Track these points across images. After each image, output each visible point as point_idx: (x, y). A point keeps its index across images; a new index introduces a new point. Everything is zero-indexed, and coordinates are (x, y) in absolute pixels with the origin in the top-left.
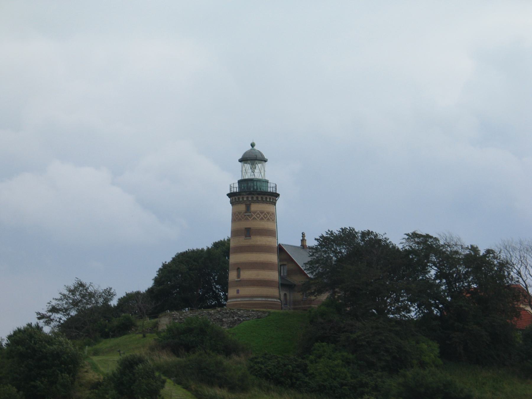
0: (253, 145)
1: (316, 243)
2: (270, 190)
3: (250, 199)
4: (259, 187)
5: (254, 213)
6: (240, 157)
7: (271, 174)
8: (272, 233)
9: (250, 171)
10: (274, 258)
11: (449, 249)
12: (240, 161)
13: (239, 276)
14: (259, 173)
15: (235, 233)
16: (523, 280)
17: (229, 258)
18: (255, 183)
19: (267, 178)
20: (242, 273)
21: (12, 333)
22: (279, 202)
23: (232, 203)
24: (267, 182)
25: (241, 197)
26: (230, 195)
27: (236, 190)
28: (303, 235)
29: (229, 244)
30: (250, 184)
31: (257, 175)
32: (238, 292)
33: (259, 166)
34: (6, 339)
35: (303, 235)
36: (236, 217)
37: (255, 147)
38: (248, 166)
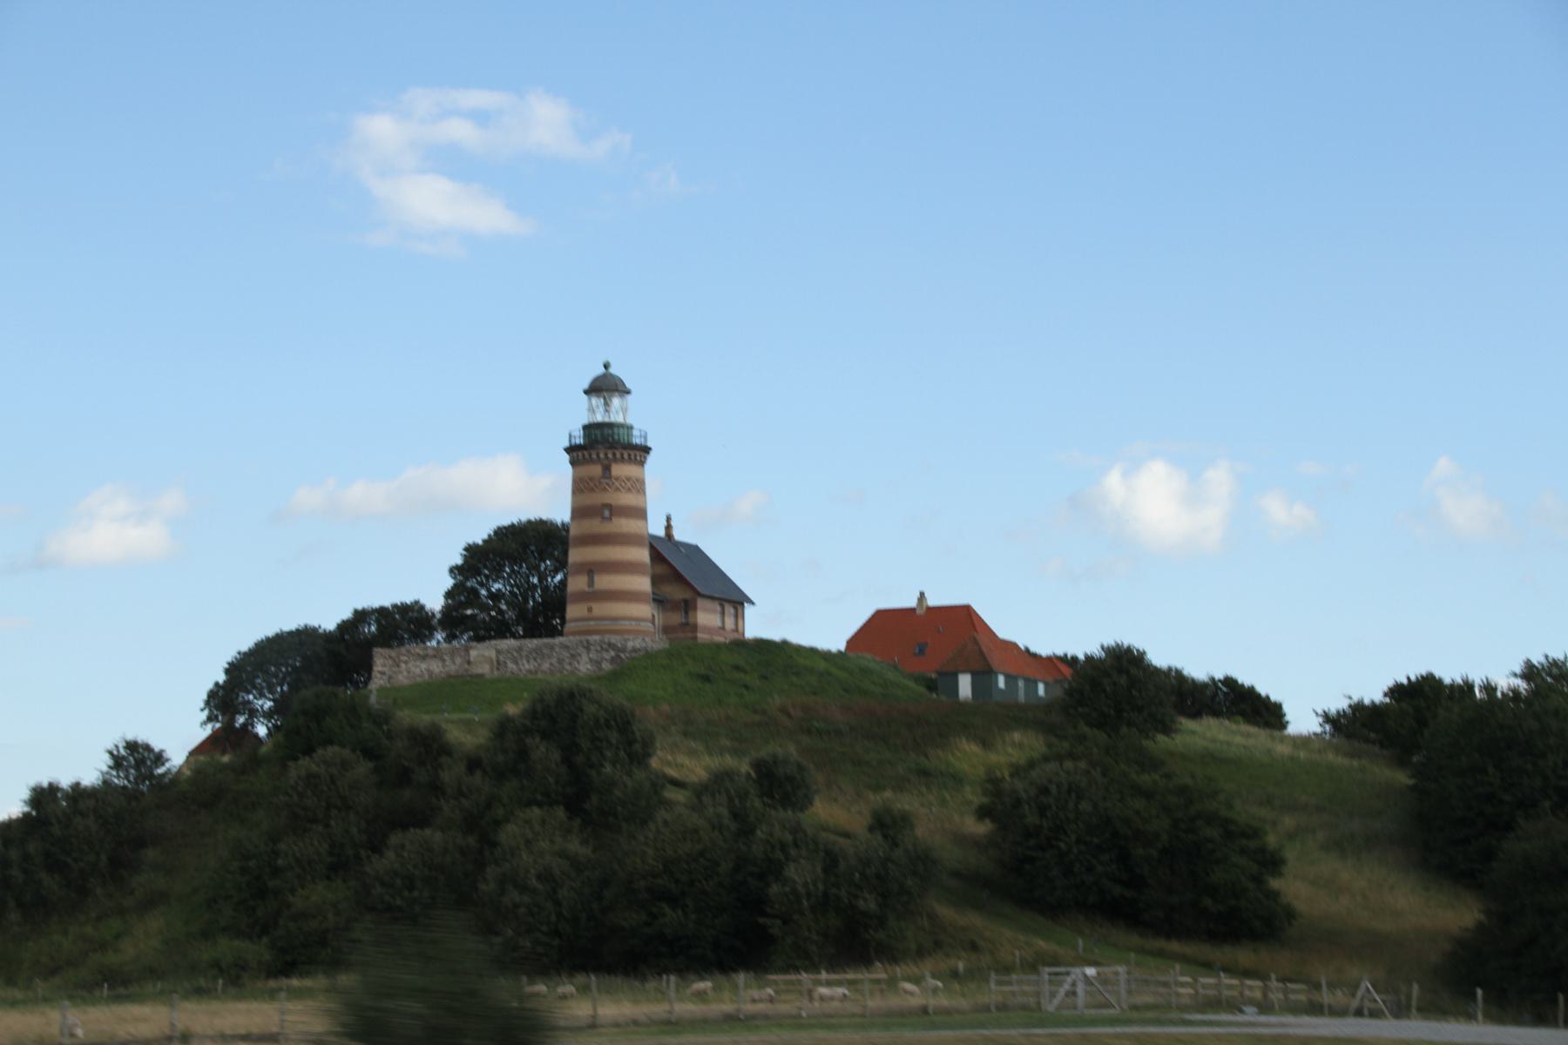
1: (206, 712)
2: (637, 440)
5: (617, 479)
6: (586, 386)
7: (629, 413)
8: (641, 513)
9: (602, 409)
10: (643, 555)
11: (1085, 806)
12: (586, 392)
13: (591, 583)
14: (617, 411)
15: (578, 512)
19: (629, 421)
20: (596, 578)
21: (221, 678)
22: (651, 459)
23: (573, 463)
24: (630, 428)
27: (579, 441)
28: (668, 519)
29: (567, 531)
30: (607, 431)
31: (617, 418)
32: (590, 610)
33: (616, 401)
35: (668, 519)
36: (579, 487)
38: (597, 401)
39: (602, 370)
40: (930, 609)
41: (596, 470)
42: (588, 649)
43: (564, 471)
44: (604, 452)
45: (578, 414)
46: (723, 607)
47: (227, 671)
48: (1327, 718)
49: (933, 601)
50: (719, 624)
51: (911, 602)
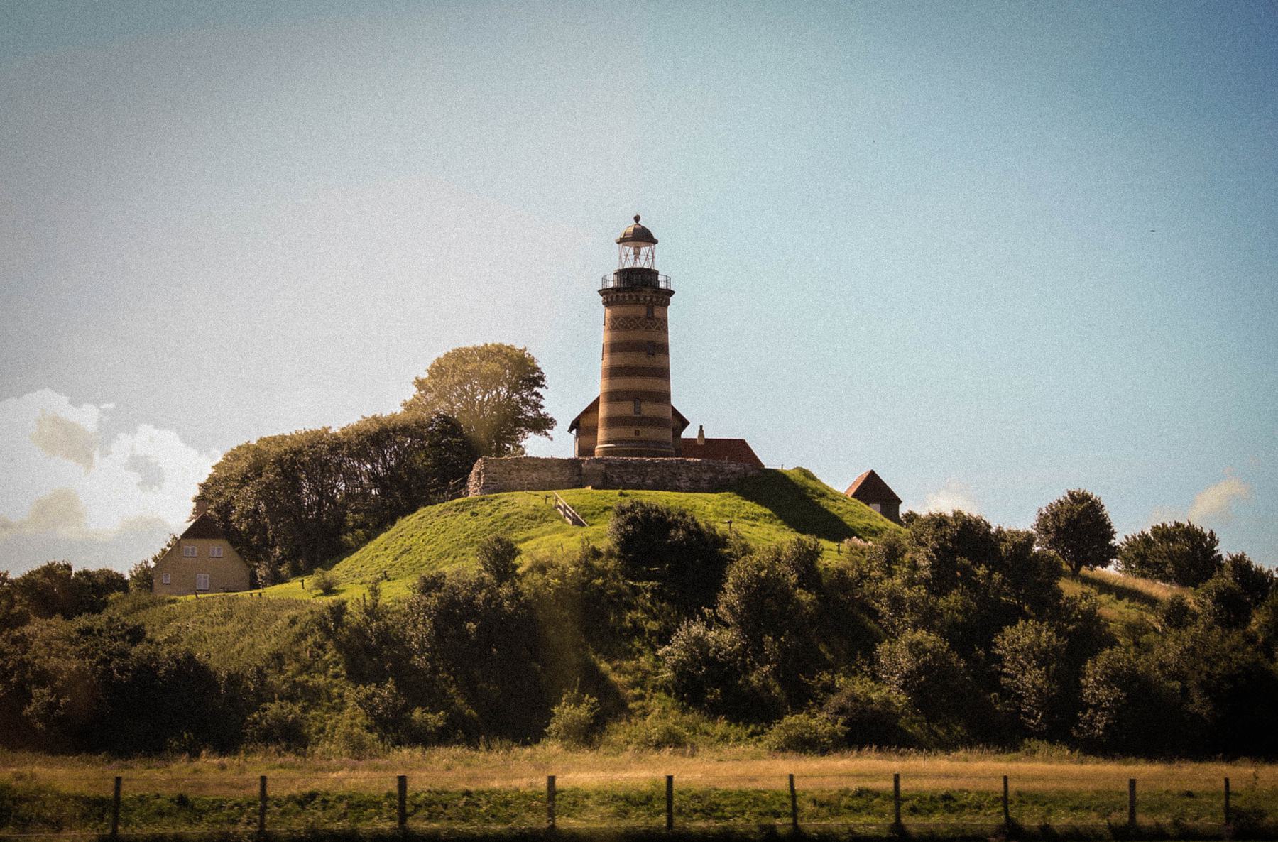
45: (610, 262)
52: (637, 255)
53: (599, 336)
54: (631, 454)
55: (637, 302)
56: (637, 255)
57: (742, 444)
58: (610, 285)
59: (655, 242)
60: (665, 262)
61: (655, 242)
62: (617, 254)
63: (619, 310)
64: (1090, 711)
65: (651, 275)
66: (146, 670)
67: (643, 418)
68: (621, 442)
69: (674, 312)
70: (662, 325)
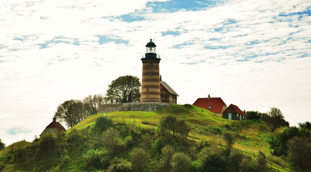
0: (151, 40)
2: (158, 57)
3: (153, 61)
4: (3, 154)
12: (146, 46)
16: (241, 61)
17: (209, 109)
18: (154, 55)
19: (156, 53)
25: (147, 60)
26: (142, 59)
34: (83, 101)
37: (152, 41)
38: (149, 49)
39: (150, 41)
40: (211, 98)
41: (149, 64)
42: (151, 105)
43: (141, 65)
44: (151, 61)
45: (144, 51)
46: (173, 96)
47: (232, 106)
48: (300, 125)
49: (211, 97)
50: (172, 100)
51: (207, 97)
52: (151, 49)
53: (124, 75)
54: (148, 102)
55: (148, 62)
56: (151, 49)
57: (220, 99)
58: (145, 57)
59: (156, 46)
60: (158, 51)
61: (156, 46)
62: (146, 49)
63: (146, 64)
64: (58, 143)
65: (155, 55)
66: (118, 146)
67: (149, 92)
68: (144, 99)
69: (161, 65)
70: (157, 68)
